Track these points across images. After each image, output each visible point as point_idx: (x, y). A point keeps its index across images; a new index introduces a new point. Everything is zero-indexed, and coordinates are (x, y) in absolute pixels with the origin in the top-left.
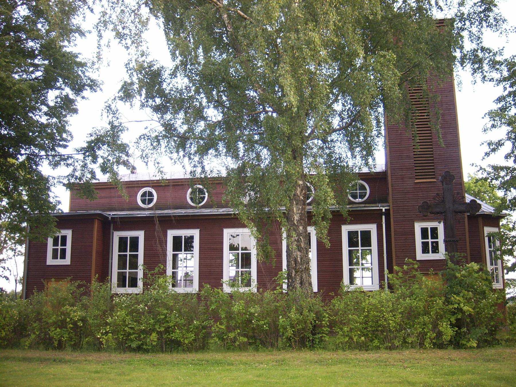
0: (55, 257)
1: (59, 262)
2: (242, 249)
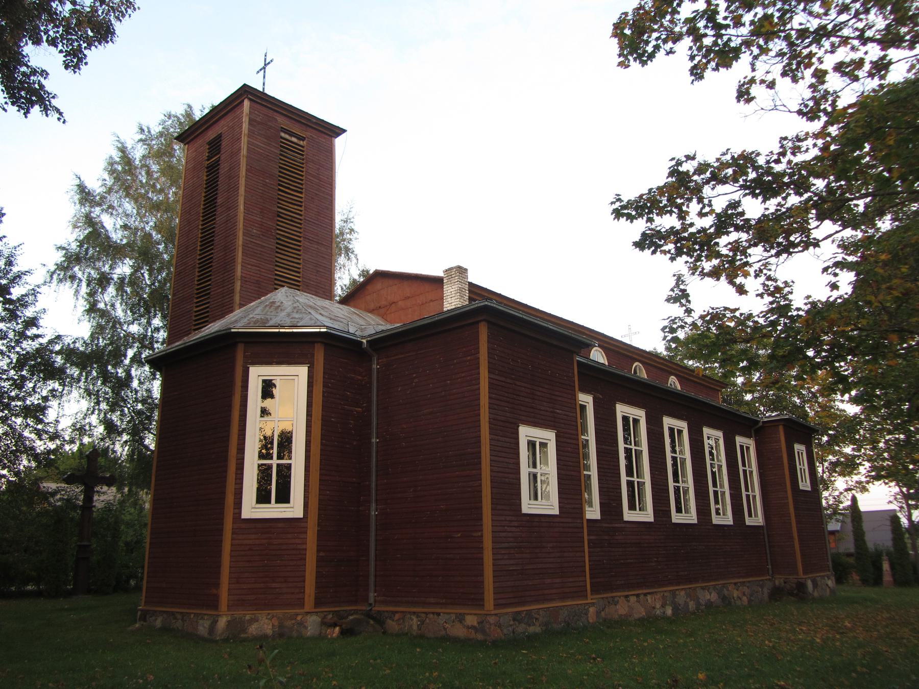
0: (263, 497)
1: (273, 511)
2: (269, 456)
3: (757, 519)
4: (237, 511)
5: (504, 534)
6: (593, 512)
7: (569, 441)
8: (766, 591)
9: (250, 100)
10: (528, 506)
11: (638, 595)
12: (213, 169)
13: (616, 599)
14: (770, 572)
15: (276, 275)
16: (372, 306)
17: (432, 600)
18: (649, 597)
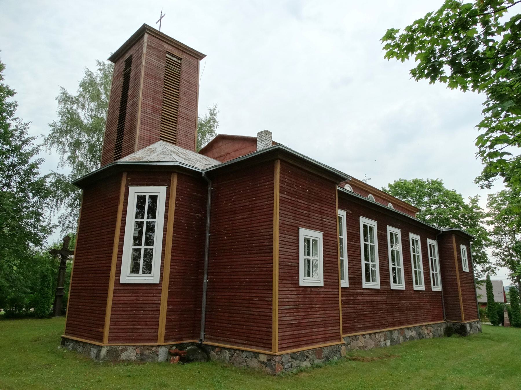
1: (141, 278)
3: (437, 288)
4: (117, 278)
5: (287, 300)
6: (345, 283)
7: (331, 239)
8: (442, 329)
9: (148, 33)
10: (304, 281)
11: (370, 334)
12: (127, 77)
13: (357, 337)
14: (445, 318)
15: (161, 136)
16: (216, 156)
17: (239, 341)
18: (377, 335)
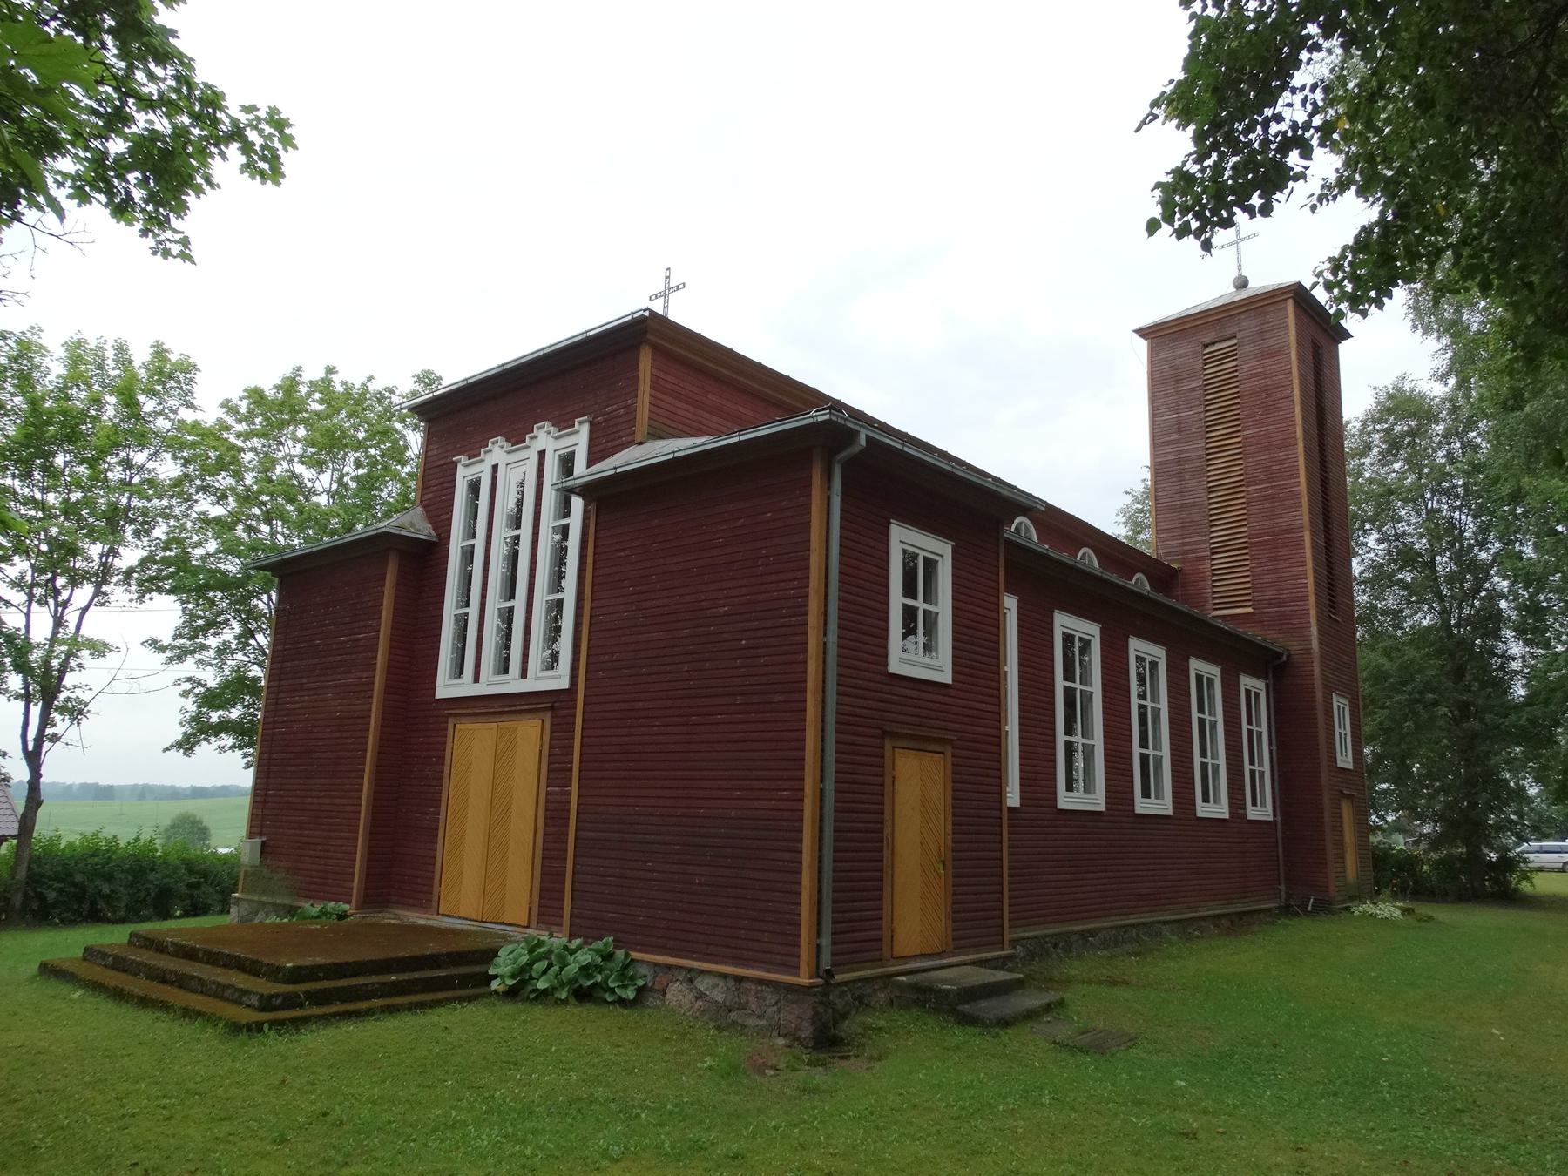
3: (1261, 811)
